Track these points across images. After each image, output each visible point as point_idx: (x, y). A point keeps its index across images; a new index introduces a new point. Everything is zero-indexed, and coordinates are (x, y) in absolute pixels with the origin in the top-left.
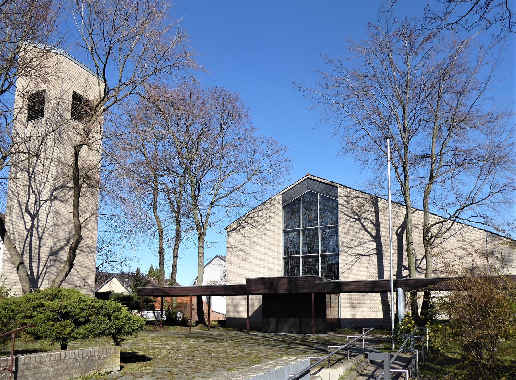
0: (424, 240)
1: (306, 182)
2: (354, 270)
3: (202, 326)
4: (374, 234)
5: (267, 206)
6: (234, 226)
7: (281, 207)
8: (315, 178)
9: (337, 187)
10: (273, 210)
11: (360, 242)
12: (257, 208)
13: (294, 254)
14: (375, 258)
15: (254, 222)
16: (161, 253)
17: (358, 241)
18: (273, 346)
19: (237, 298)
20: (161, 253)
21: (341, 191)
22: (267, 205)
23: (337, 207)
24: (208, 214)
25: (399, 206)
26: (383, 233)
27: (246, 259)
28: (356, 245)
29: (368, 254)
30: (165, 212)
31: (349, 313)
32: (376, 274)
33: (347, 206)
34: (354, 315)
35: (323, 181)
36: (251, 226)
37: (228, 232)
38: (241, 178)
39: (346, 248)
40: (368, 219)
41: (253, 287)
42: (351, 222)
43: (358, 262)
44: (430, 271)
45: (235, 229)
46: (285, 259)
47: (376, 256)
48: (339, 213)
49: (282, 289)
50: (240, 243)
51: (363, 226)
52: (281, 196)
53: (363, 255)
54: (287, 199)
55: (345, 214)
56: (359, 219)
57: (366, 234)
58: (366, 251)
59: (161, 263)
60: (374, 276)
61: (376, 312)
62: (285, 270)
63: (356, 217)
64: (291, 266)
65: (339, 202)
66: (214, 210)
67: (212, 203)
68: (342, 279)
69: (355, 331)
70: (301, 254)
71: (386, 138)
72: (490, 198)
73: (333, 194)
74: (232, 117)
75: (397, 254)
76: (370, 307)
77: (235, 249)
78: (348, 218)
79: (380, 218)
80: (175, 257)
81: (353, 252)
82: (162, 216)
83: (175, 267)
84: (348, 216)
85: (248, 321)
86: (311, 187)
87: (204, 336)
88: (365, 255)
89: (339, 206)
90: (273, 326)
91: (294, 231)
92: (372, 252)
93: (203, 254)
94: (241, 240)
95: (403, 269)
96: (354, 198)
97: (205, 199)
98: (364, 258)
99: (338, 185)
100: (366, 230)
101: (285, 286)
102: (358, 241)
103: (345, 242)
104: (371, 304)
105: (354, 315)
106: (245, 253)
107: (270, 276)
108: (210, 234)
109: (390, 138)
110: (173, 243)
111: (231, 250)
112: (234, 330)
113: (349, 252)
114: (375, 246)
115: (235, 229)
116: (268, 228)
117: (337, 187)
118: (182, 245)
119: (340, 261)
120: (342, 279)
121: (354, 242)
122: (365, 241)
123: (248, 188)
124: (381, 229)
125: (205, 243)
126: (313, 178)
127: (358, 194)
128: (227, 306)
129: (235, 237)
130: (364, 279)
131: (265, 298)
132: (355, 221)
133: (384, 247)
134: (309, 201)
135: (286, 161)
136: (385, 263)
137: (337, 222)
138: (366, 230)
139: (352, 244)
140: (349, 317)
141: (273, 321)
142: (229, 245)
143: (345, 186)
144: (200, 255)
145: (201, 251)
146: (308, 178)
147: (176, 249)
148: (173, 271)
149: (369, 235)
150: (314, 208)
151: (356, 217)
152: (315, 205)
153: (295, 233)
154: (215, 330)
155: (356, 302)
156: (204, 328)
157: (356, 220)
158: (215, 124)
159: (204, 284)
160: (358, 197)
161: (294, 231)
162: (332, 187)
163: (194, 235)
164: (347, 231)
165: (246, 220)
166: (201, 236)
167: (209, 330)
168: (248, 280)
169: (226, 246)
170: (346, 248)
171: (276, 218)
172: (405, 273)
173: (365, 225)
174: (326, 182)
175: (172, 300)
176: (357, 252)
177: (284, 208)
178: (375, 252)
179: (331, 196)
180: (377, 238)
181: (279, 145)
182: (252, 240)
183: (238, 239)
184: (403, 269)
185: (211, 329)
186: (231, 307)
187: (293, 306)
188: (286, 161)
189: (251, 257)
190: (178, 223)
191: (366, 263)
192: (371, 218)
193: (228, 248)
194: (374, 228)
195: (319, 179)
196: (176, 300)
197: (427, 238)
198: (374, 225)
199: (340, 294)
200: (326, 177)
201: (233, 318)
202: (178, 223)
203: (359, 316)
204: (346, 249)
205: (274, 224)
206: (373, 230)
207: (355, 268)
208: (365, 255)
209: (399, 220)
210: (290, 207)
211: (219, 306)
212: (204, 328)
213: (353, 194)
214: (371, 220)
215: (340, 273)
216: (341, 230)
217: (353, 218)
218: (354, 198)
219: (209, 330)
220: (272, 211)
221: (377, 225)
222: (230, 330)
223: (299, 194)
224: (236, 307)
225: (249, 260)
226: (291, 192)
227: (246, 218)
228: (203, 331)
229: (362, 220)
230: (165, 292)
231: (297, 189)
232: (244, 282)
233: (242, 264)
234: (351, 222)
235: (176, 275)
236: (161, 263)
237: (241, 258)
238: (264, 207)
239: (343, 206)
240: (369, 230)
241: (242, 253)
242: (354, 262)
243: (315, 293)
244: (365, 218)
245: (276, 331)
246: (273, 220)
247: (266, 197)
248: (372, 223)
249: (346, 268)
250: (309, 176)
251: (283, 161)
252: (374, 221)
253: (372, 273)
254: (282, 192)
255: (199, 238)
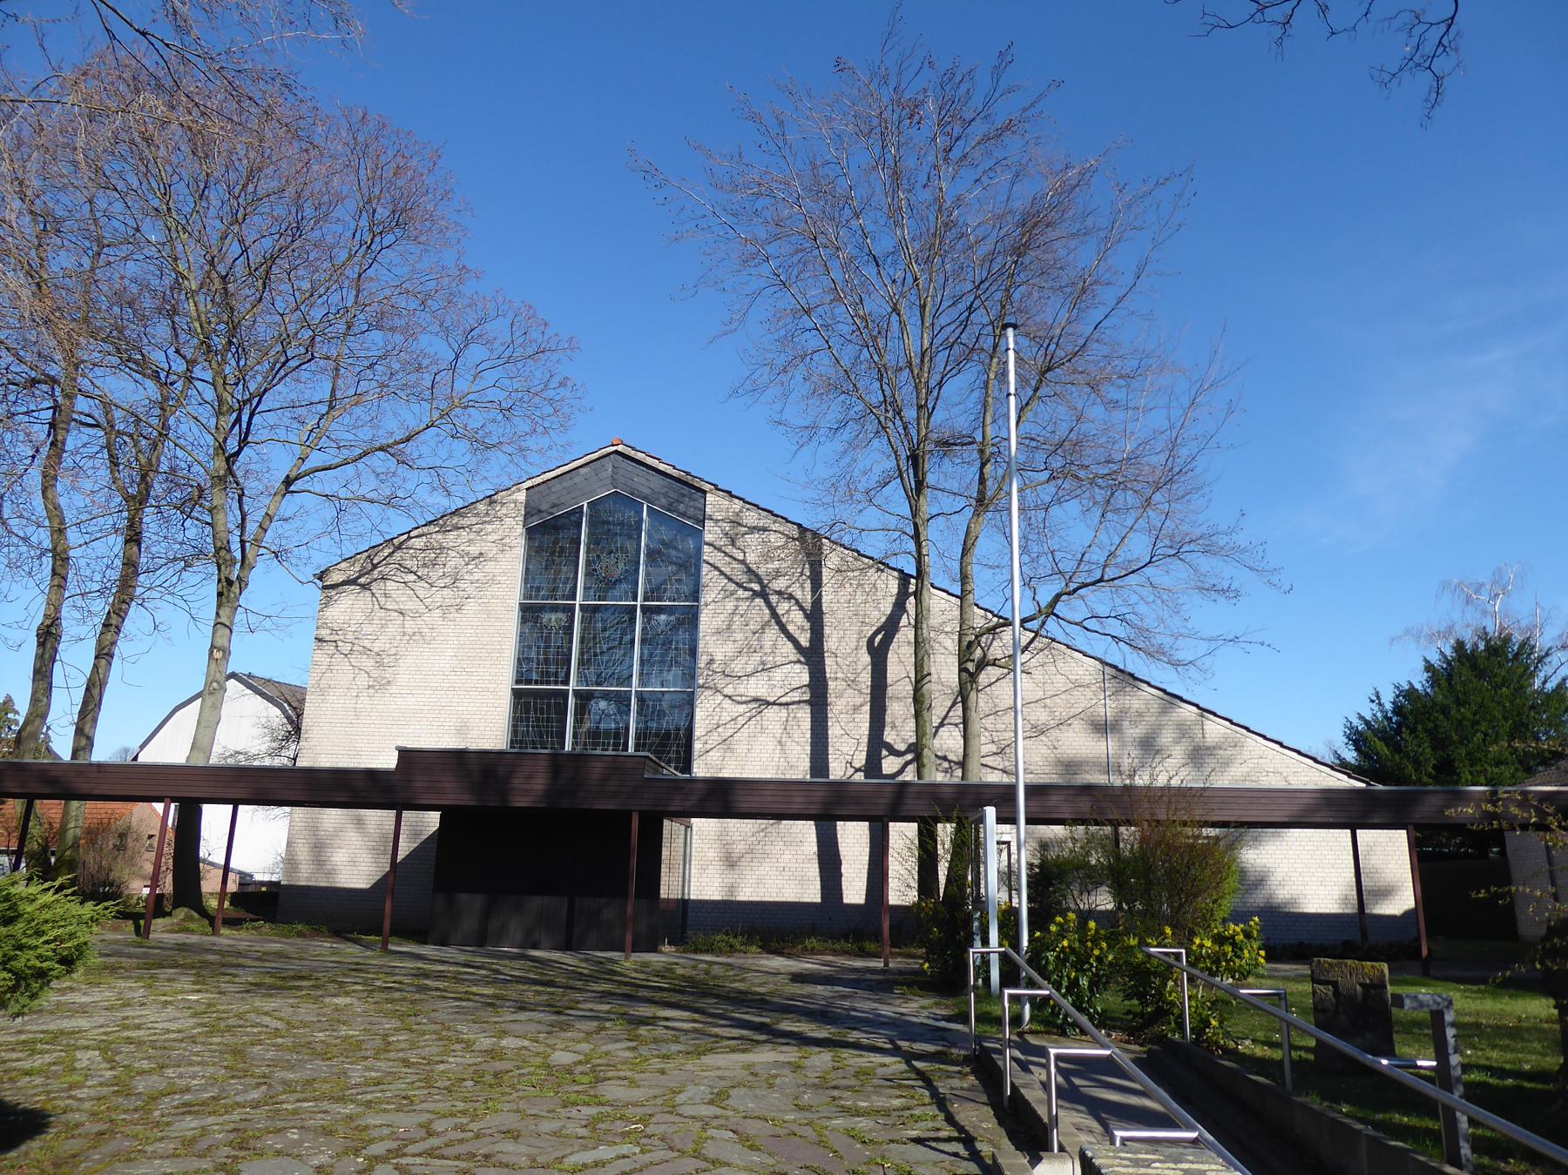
0: (961, 670)
1: (608, 465)
2: (741, 748)
3: (188, 918)
4: (804, 640)
5: (474, 520)
6: (352, 572)
7: (520, 529)
8: (640, 456)
9: (705, 492)
10: (494, 531)
11: (763, 663)
12: (444, 521)
13: (548, 683)
14: (804, 715)
15: (425, 565)
16: (48, 636)
17: (756, 658)
18: (492, 1004)
19: (332, 817)
20: (48, 636)
21: (715, 503)
22: (477, 515)
23: (699, 551)
24: (269, 517)
25: (879, 569)
26: (832, 641)
27: (380, 685)
28: (749, 669)
29: (783, 700)
30: (88, 491)
31: (717, 882)
32: (805, 763)
33: (729, 549)
34: (732, 888)
35: (662, 467)
36: (412, 577)
37: (325, 587)
38: (400, 416)
39: (718, 677)
40: (791, 597)
41: (419, 783)
42: (738, 599)
43: (752, 722)
44: (973, 765)
45: (353, 582)
46: (517, 694)
47: (808, 709)
48: (705, 569)
49: (529, 790)
50: (367, 629)
51: (774, 614)
52: (524, 493)
53: (768, 703)
54: (543, 508)
55: (722, 573)
56: (763, 594)
57: (783, 640)
58: (780, 692)
59: (43, 674)
60: (798, 767)
61: (802, 881)
62: (515, 732)
63: (756, 587)
64: (537, 719)
65: (708, 537)
66: (290, 505)
67: (288, 482)
68: (700, 770)
69: (749, 942)
70: (572, 686)
71: (1005, 327)
72: (1149, 571)
73: (691, 512)
74: (400, 218)
75: (867, 708)
76: (776, 866)
77: (346, 648)
78: (732, 587)
79: (826, 599)
80: (104, 654)
81: (741, 690)
82: (71, 502)
83: (96, 692)
84: (730, 580)
85: (388, 905)
86: (622, 480)
87: (211, 957)
88: (774, 703)
89: (706, 548)
90: (469, 923)
91: (555, 608)
92: (796, 696)
93: (226, 652)
94: (369, 618)
95: (884, 753)
96: (754, 529)
97: (268, 461)
98: (771, 712)
99: (707, 487)
100: (783, 628)
101: (539, 783)
102: (756, 658)
103: (719, 657)
104: (787, 857)
105: (732, 888)
106: (380, 664)
107: (462, 746)
108: (266, 585)
109: (1015, 327)
110: (100, 607)
111: (330, 648)
112: (316, 933)
113: (729, 691)
114: (805, 678)
115: (353, 582)
116: (471, 589)
117: (705, 492)
118: (136, 619)
119: (699, 715)
120: (700, 770)
121: (743, 660)
122: (779, 660)
123: (425, 450)
124: (827, 631)
125: (240, 616)
126: (632, 453)
127: (766, 521)
128: (289, 844)
129: (348, 608)
130: (769, 775)
131: (450, 816)
132: (752, 599)
133: (831, 685)
134: (612, 523)
135: (561, 385)
136: (834, 731)
137: (695, 595)
138: (783, 628)
139: (737, 667)
140: (717, 897)
141: (471, 904)
142: (324, 633)
143: (729, 493)
144: (217, 655)
145: (219, 642)
146: (616, 452)
147: (112, 626)
148: (85, 703)
149: (790, 645)
150: (629, 545)
151: (756, 587)
152: (630, 537)
153: (560, 615)
154: (243, 934)
155: (739, 848)
156: (192, 926)
157: (755, 594)
158: (341, 227)
159: (214, 761)
160: (765, 529)
161: (555, 608)
162: (689, 488)
163: (202, 587)
164: (722, 625)
165: (398, 555)
166: (228, 590)
167: (215, 933)
168: (405, 754)
169: (314, 633)
170: (718, 677)
171: (500, 564)
172: (890, 765)
173: (780, 612)
174: (670, 470)
175: (66, 813)
176: (753, 693)
177: (531, 533)
178: (807, 697)
179: (684, 515)
180: (813, 655)
181: (549, 332)
182: (409, 623)
183: (359, 616)
184: (884, 753)
185: (224, 931)
186: (303, 853)
187: (539, 851)
188: (561, 385)
189: (402, 679)
190: (134, 537)
191: (777, 729)
192: (798, 594)
193: (320, 640)
194: (807, 625)
195: (649, 461)
196: (83, 813)
197: (971, 667)
198: (807, 617)
199: (693, 820)
200: (674, 456)
201: (327, 888)
202: (134, 537)
203: (746, 894)
204: (720, 681)
205: (492, 580)
206: (802, 629)
207: (746, 736)
208: (774, 703)
209: (877, 608)
210: (549, 535)
211: (254, 843)
212: (192, 926)
213: (751, 518)
214: (797, 602)
215: (696, 754)
216: (708, 621)
217: (746, 589)
218: (754, 529)
219: (215, 933)
220: (490, 538)
221: (815, 616)
222: (300, 935)
223: (584, 496)
224: (319, 849)
225: (393, 689)
226: (559, 487)
227: (399, 548)
228: (194, 939)
229: (774, 599)
230: (54, 781)
231: (577, 480)
232: (389, 761)
233: (364, 700)
234: (738, 599)
235: (95, 721)
236: (43, 674)
237: (363, 680)
238: (466, 522)
239: (719, 550)
240: (791, 628)
241: (368, 663)
242: (741, 721)
243: (641, 813)
244: (779, 593)
245: (481, 940)
246: (490, 567)
247: (484, 489)
248: (802, 608)
249: (715, 738)
250: (620, 448)
251: (554, 383)
252: (808, 606)
253: (793, 761)
254: (529, 484)
255: (220, 594)
